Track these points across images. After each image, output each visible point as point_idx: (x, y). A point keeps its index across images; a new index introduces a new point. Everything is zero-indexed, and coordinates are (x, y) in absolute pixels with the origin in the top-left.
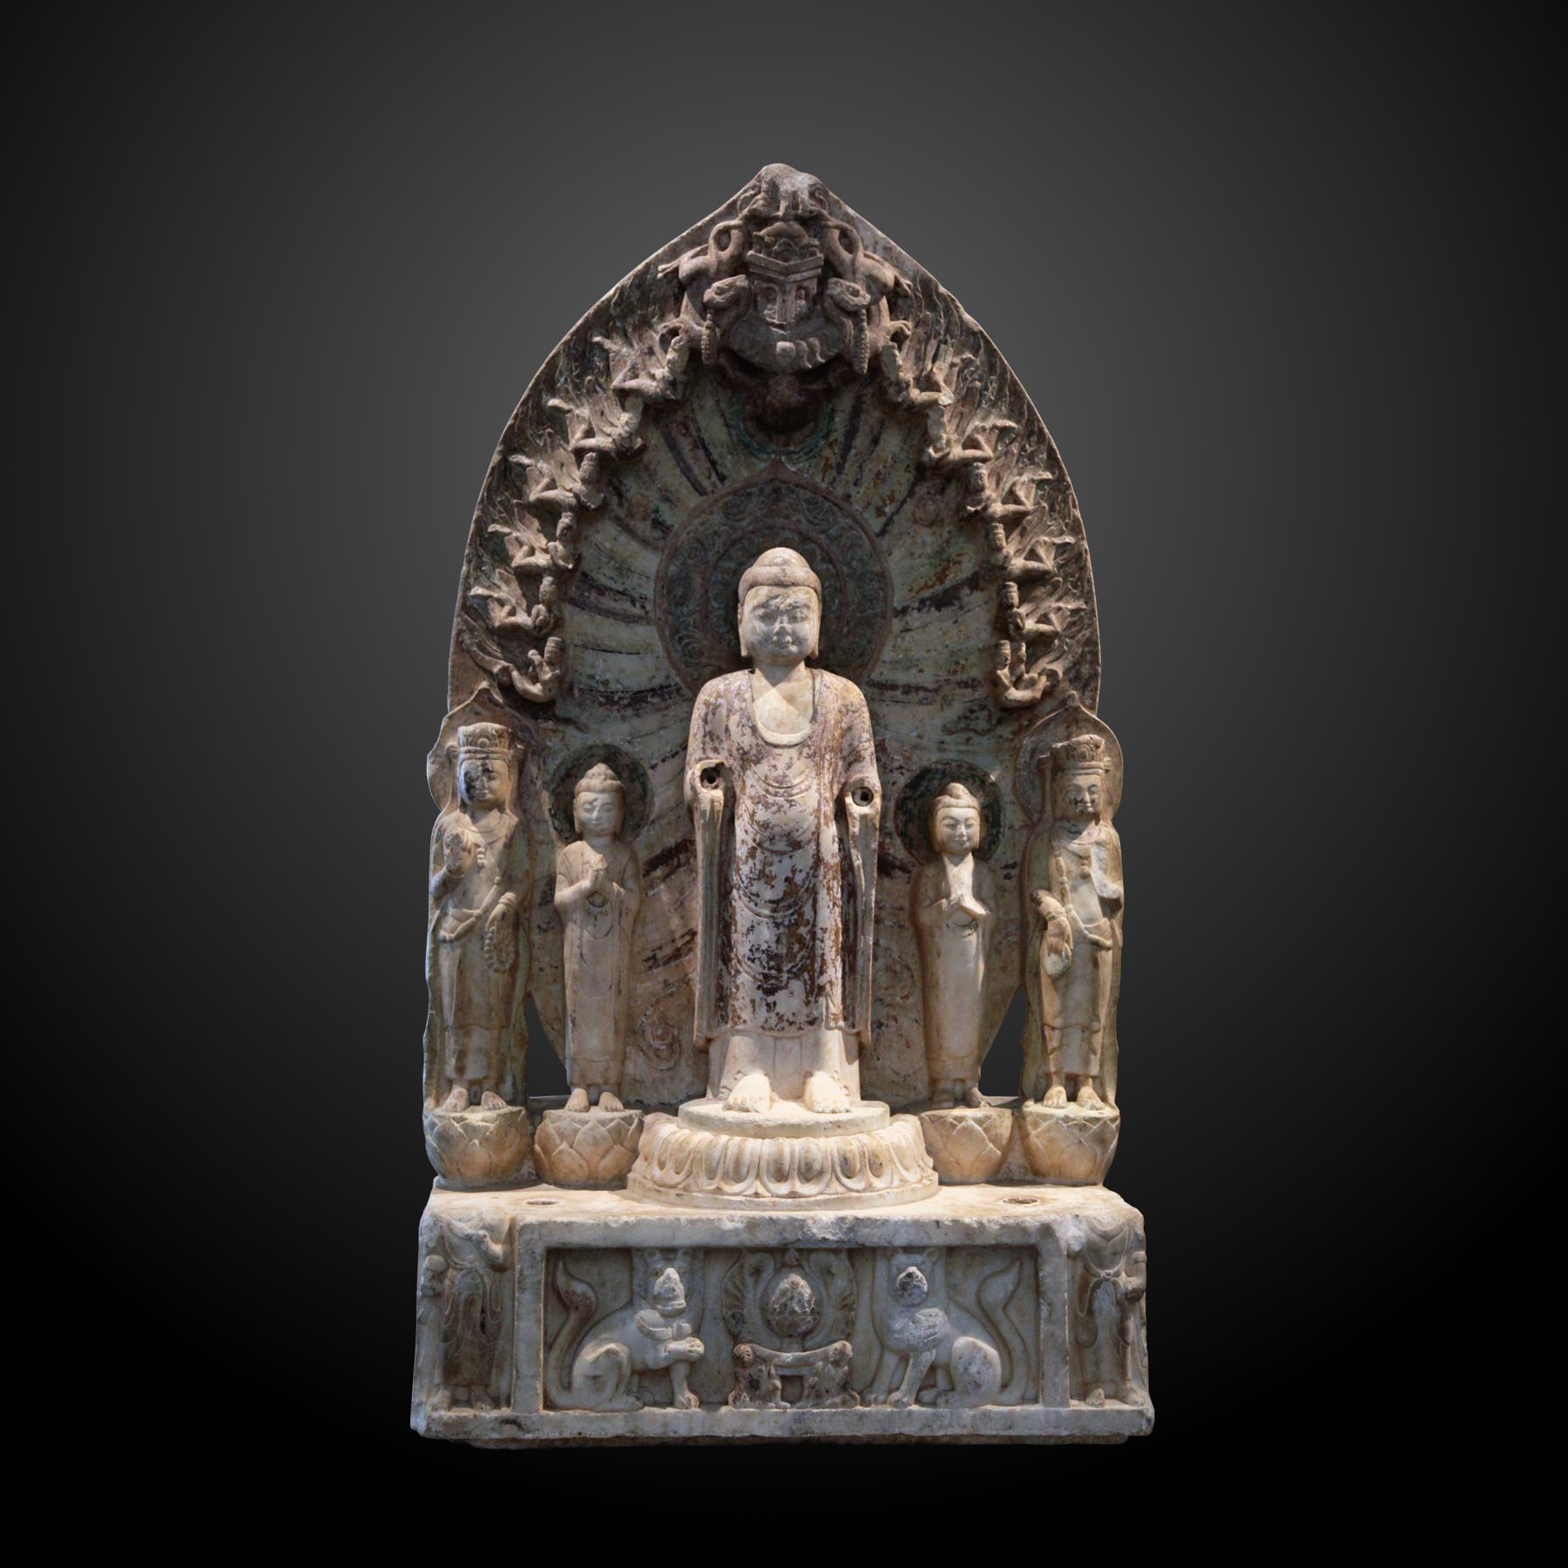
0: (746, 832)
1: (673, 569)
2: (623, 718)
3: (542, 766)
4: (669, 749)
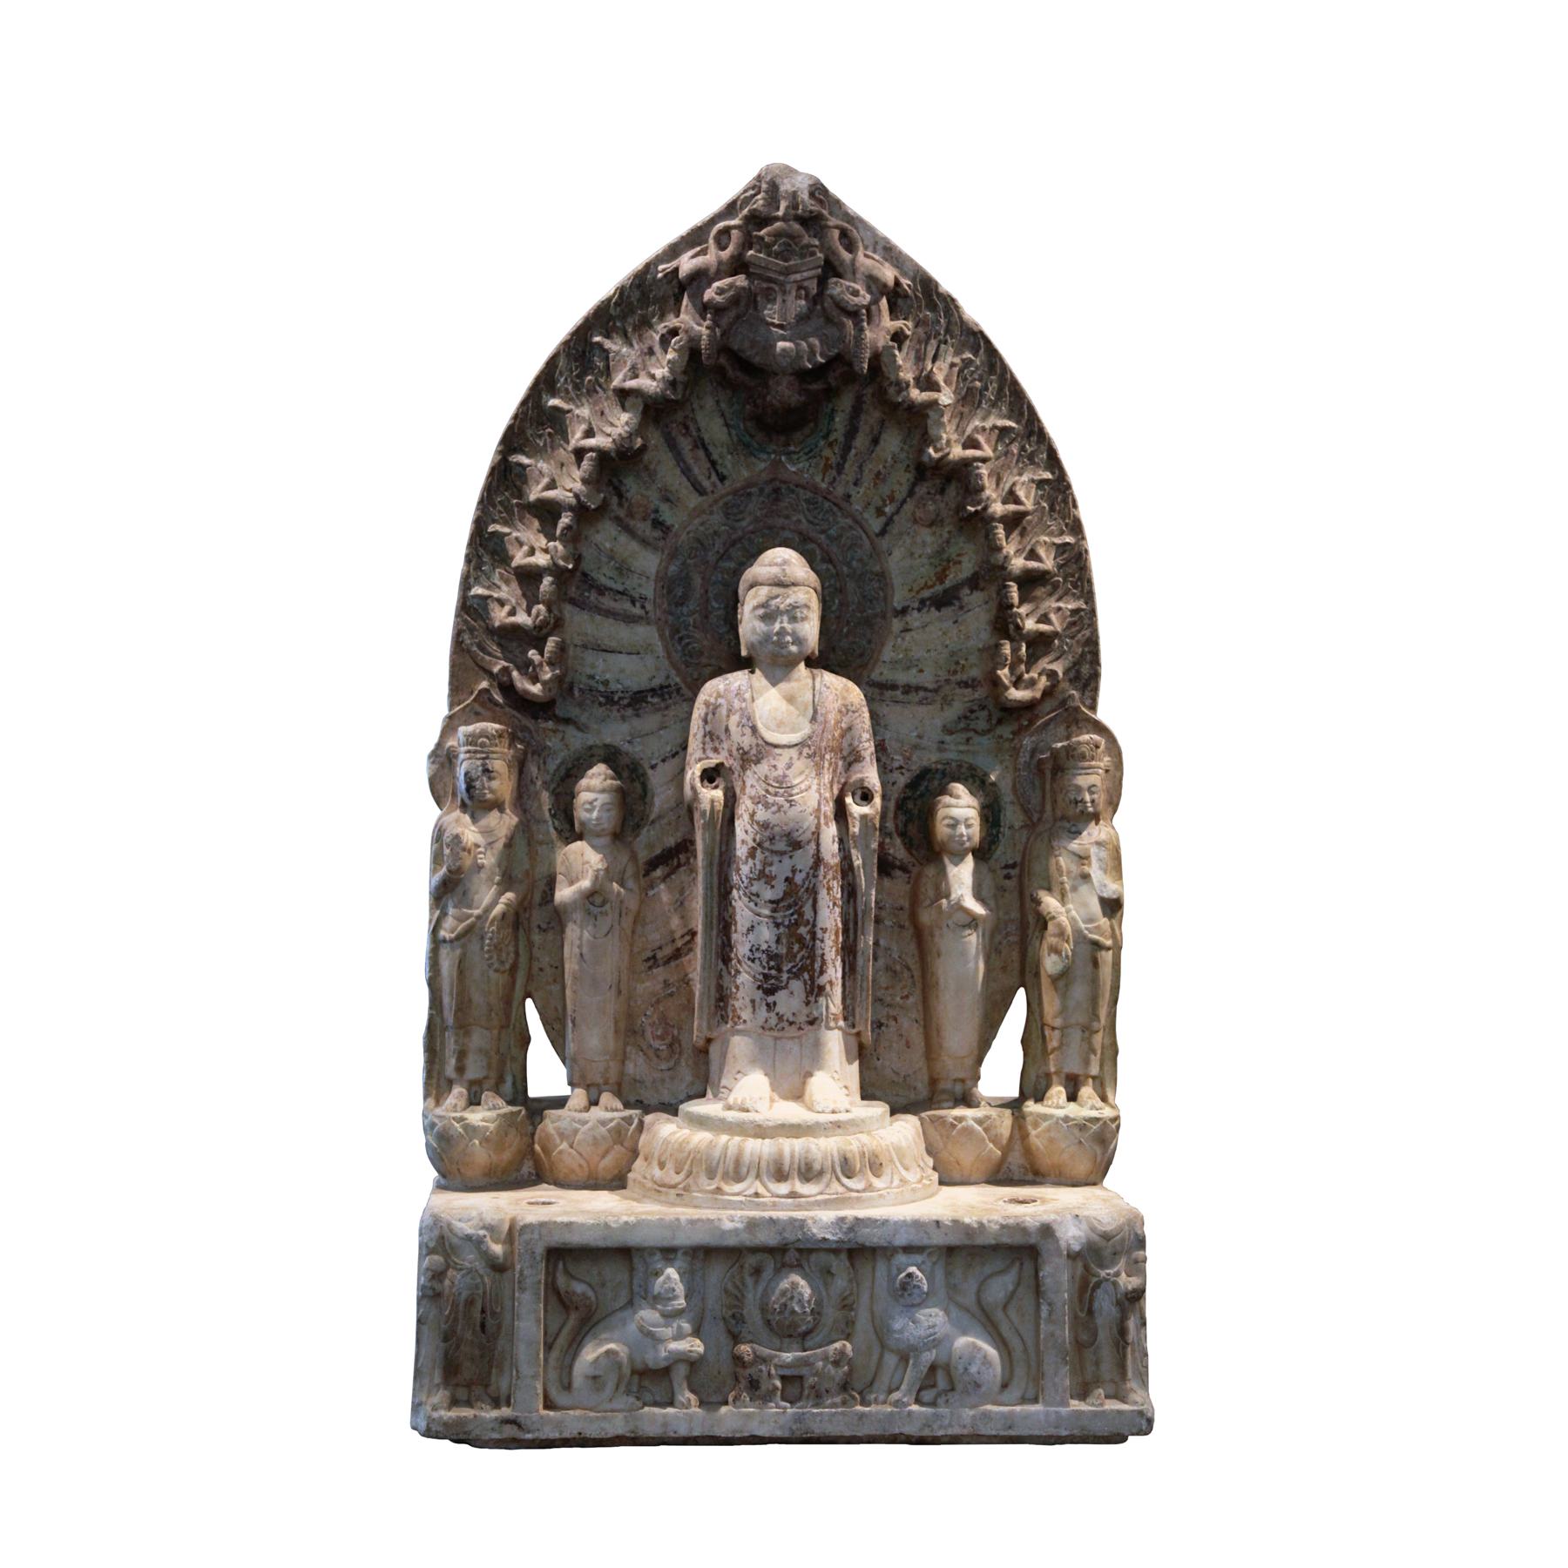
0: (746, 832)
1: (673, 569)
2: (623, 718)
3: (542, 766)
4: (669, 749)
